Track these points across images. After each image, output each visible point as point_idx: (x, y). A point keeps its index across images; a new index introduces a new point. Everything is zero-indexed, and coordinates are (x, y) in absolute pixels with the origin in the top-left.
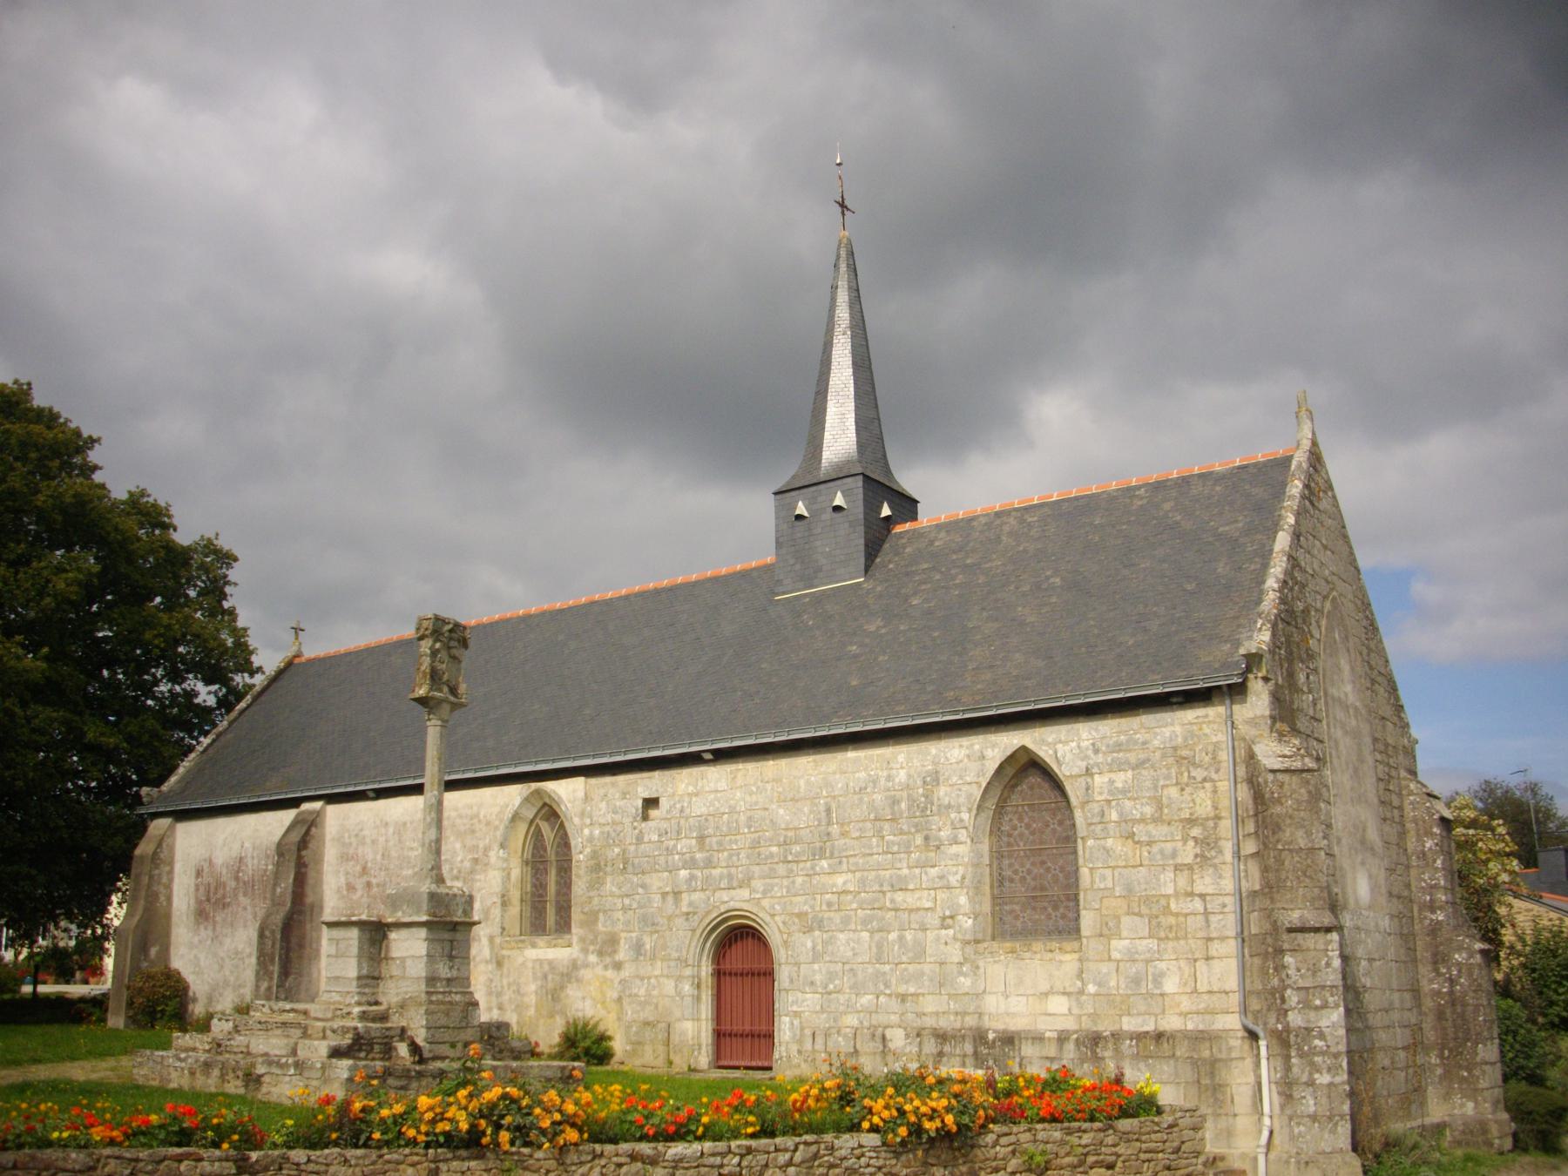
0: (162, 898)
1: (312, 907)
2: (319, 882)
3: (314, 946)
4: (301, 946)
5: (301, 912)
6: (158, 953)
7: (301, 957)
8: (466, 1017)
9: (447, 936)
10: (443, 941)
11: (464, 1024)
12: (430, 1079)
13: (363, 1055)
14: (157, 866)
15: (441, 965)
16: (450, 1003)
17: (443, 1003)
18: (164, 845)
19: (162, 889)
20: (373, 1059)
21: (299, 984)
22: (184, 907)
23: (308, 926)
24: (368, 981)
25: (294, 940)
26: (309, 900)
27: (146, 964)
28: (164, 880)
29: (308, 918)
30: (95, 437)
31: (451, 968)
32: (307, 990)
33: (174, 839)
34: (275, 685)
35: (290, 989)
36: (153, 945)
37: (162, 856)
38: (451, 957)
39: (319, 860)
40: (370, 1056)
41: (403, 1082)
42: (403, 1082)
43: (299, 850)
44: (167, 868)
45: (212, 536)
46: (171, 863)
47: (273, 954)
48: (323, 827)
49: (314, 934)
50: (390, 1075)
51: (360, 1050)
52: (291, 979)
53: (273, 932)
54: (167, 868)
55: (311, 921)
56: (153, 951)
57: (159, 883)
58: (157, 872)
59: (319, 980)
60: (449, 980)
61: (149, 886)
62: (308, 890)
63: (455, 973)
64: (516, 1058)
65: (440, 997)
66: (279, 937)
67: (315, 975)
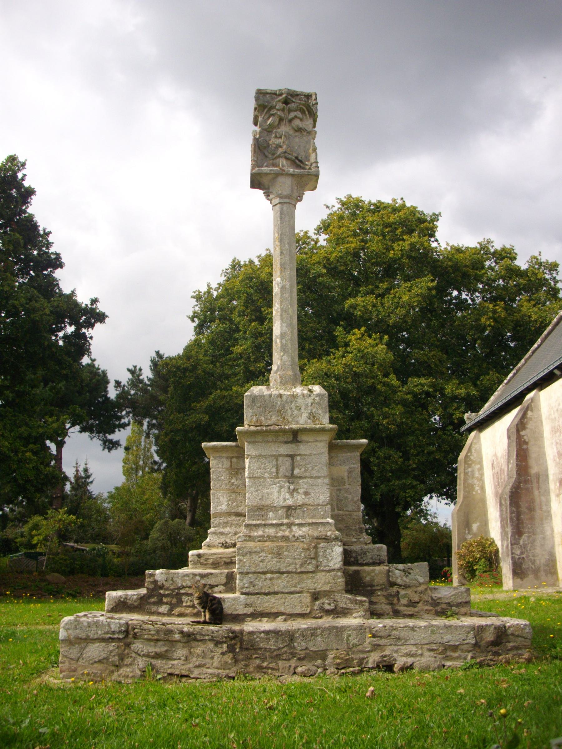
0: (477, 488)
1: (538, 476)
2: (542, 455)
3: (544, 508)
4: (531, 509)
5: (526, 482)
6: (479, 528)
7: (532, 519)
8: (316, 557)
9: (284, 449)
10: (277, 457)
11: (310, 568)
12: (211, 645)
13: (164, 609)
14: (470, 466)
15: (275, 489)
16: (285, 539)
17: (270, 538)
18: (473, 450)
19: (475, 481)
20: (181, 615)
21: (534, 541)
22: (490, 492)
23: (536, 493)
24: (233, 518)
25: (524, 505)
26: (534, 470)
27: (470, 536)
28: (477, 474)
29: (535, 485)
30: (437, 213)
31: (292, 492)
32: (542, 545)
33: (481, 444)
34: (558, 327)
35: (525, 546)
36: (474, 522)
37: (472, 458)
38: (292, 478)
39: (539, 437)
40: (177, 611)
41: (161, 648)
42: (161, 648)
43: (518, 431)
44: (478, 466)
45: (536, 254)
46: (481, 463)
47: (507, 517)
48: (539, 410)
49: (543, 498)
50: (135, 636)
51: (160, 603)
52: (524, 537)
53: (505, 500)
54: (478, 466)
55: (538, 488)
56: (475, 527)
57: (473, 477)
58: (470, 470)
59: (553, 537)
60: (289, 508)
61: (465, 480)
62: (532, 462)
63: (300, 499)
64: (442, 613)
65: (271, 531)
66: (508, 503)
67: (548, 533)
